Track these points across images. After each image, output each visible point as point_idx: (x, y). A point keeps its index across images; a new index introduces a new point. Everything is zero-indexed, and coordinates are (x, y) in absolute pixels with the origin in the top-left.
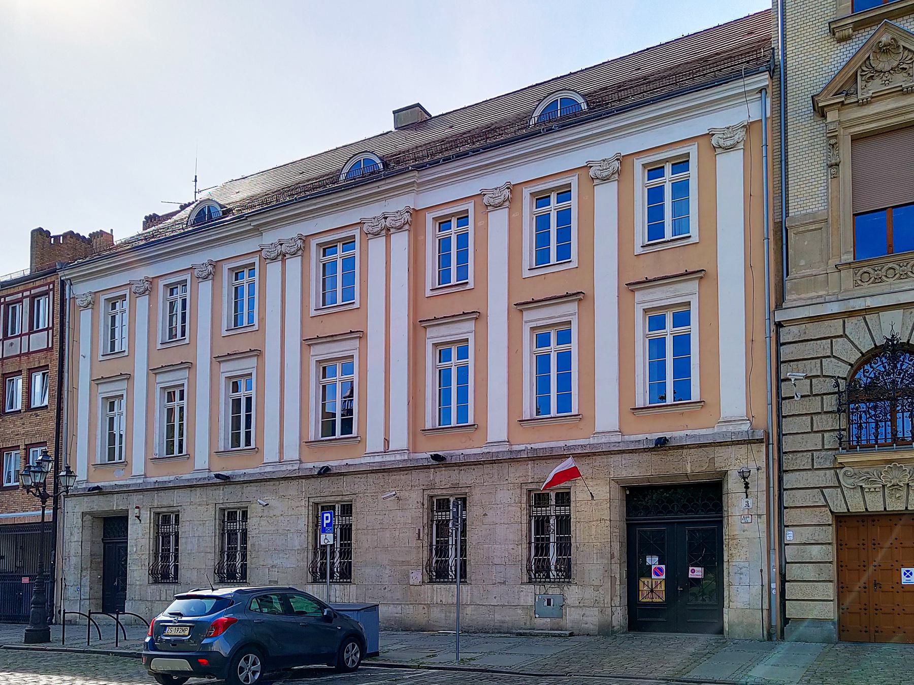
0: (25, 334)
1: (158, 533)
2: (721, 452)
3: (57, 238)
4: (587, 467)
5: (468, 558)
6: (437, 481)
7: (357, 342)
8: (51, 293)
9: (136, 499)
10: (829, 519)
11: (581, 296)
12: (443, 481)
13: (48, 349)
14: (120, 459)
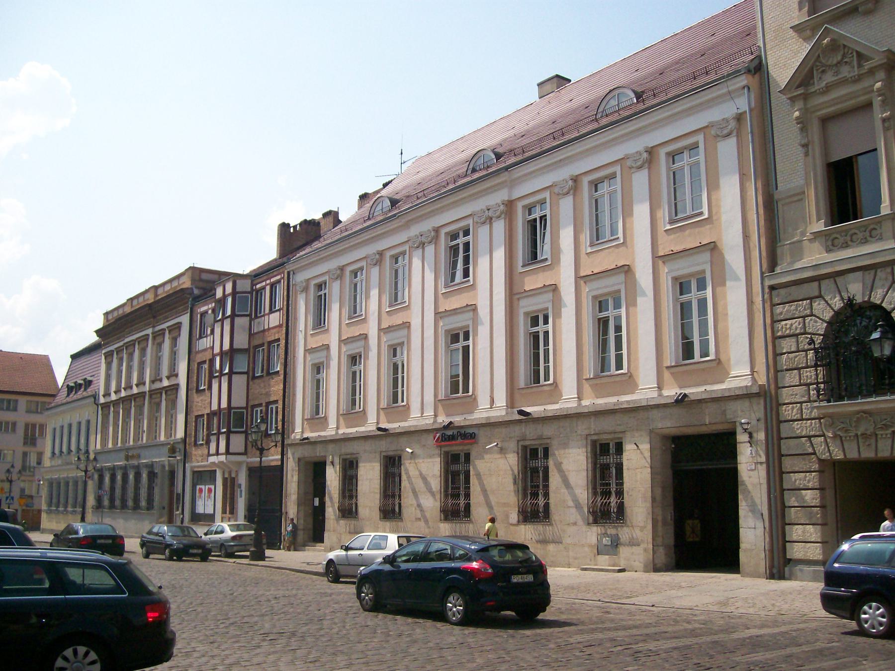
1: (526, 468)
3: (295, 227)
5: (472, 502)
6: (528, 433)
9: (331, 447)
10: (816, 466)
11: (626, 268)
13: (280, 326)
14: (403, 401)
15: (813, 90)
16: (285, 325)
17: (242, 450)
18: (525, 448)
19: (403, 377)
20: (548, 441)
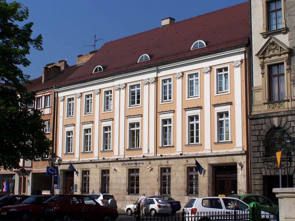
0: (43, 109)
2: (236, 157)
4: (202, 160)
5: (140, 188)
6: (163, 163)
7: (140, 118)
8: (51, 95)
11: (201, 107)
12: (105, 166)
13: (50, 114)
15: (266, 56)
16: (53, 114)
17: (30, 166)
18: (161, 168)
19: (90, 141)
20: (89, 169)
